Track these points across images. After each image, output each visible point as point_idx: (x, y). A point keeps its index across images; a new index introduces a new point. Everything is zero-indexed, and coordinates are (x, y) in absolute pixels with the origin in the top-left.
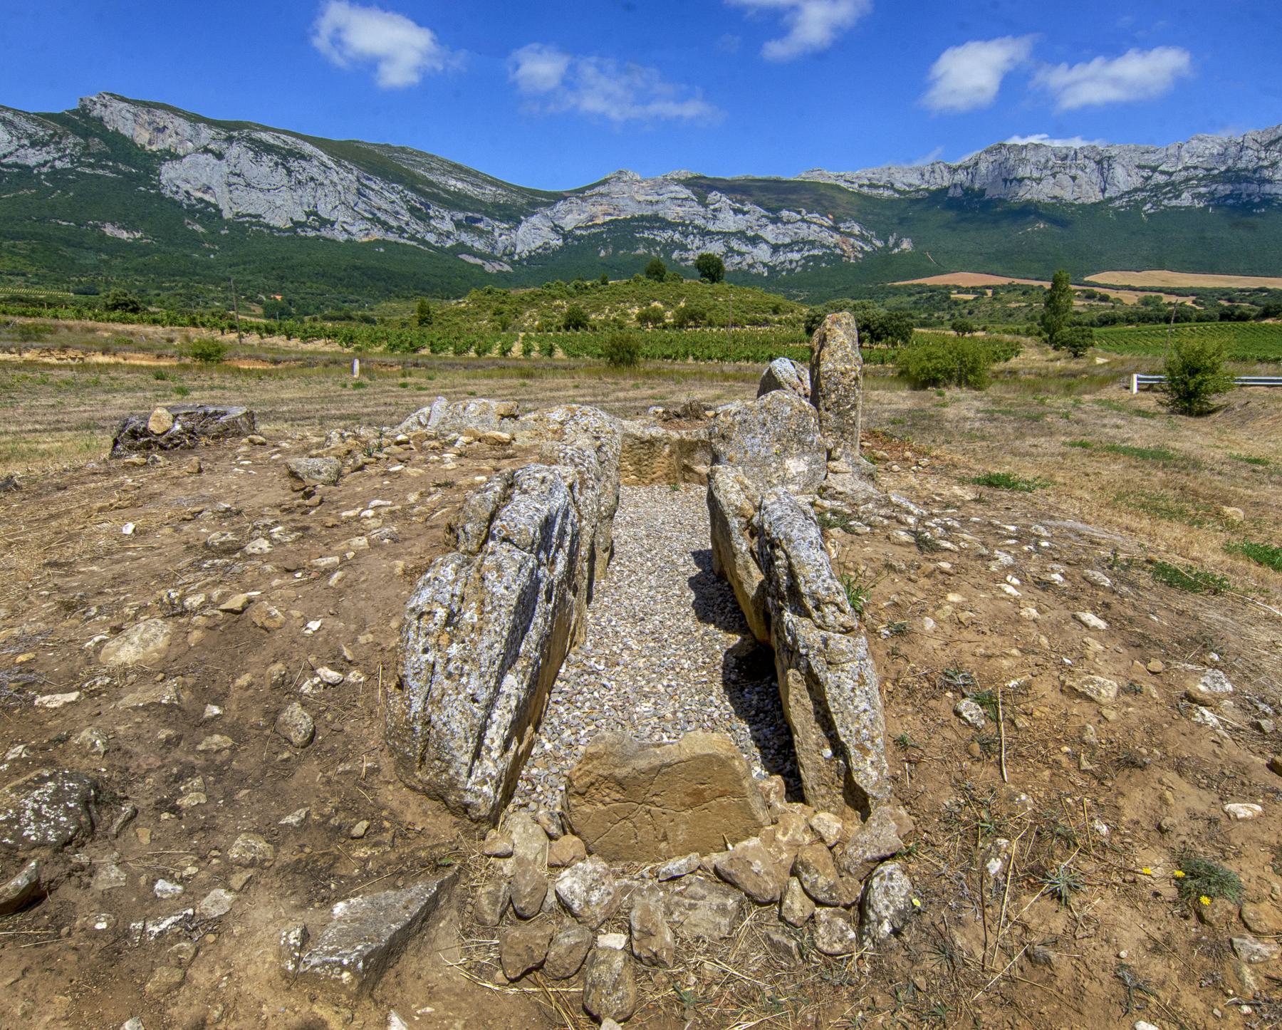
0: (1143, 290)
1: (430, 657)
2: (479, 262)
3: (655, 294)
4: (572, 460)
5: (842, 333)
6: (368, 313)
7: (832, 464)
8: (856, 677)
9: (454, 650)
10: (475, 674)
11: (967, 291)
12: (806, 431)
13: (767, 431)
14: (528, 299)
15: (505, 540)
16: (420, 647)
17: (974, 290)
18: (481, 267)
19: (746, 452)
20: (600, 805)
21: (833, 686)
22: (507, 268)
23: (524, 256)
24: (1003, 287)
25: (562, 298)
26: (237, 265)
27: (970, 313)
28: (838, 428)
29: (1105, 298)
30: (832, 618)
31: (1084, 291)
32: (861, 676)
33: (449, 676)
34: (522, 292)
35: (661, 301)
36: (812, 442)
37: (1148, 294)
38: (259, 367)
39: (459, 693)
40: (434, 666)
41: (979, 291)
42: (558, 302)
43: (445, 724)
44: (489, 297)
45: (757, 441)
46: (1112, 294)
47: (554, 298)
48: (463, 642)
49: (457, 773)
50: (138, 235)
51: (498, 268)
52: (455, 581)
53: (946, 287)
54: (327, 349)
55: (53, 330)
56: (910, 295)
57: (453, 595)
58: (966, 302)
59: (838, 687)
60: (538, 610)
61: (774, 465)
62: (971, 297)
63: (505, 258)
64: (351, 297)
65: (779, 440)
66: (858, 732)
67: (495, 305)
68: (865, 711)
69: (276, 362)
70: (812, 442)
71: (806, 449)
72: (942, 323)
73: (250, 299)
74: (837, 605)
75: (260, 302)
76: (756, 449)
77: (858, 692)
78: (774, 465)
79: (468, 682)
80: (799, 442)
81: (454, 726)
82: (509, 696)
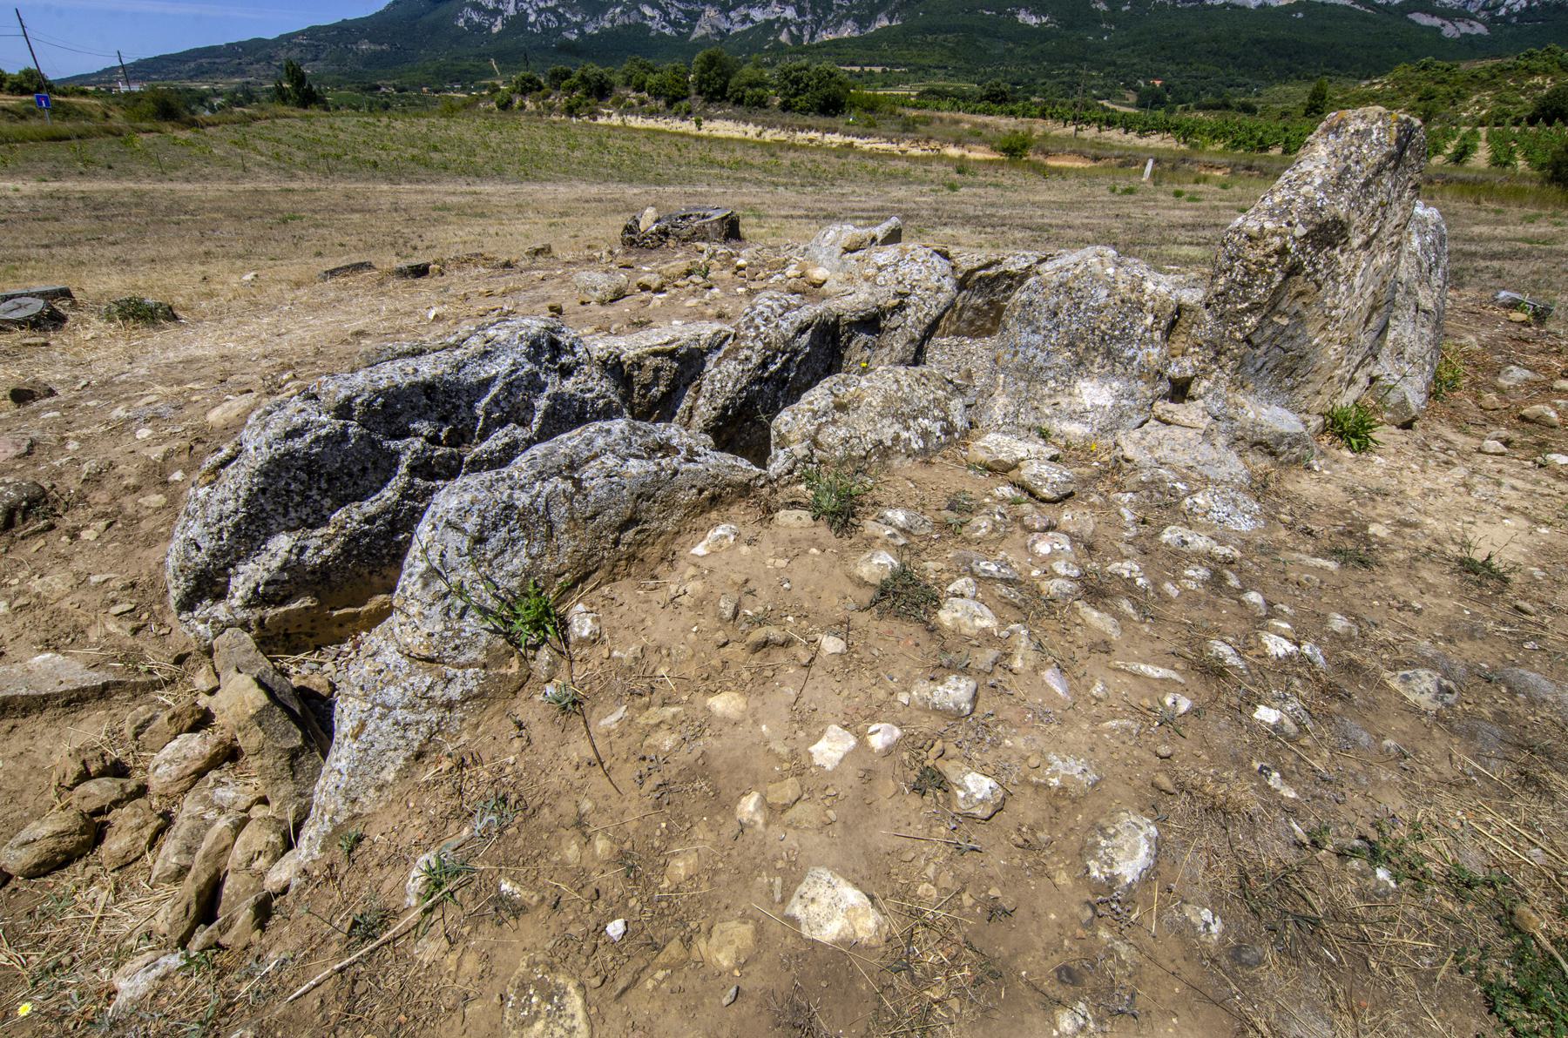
2: (1437, 22)
6: (1252, 100)
12: (1126, 337)
14: (1485, 75)
18: (1438, 30)
19: (1015, 354)
22: (1480, 29)
23: (1517, 8)
26: (1128, 46)
28: (1211, 343)
34: (1477, 65)
36: (1133, 358)
38: (1079, 164)
42: (1538, 80)
44: (1421, 74)
47: (1533, 73)
50: (1044, 20)
51: (1464, 28)
54: (1161, 145)
55: (927, 122)
60: (393, 482)
61: (1052, 384)
63: (1483, 14)
64: (1240, 80)
65: (1072, 344)
67: (1426, 85)
69: (1096, 159)
70: (1133, 358)
71: (1119, 369)
73: (1128, 86)
75: (1136, 90)
76: (1030, 352)
78: (1052, 384)
80: (1108, 354)
82: (274, 555)
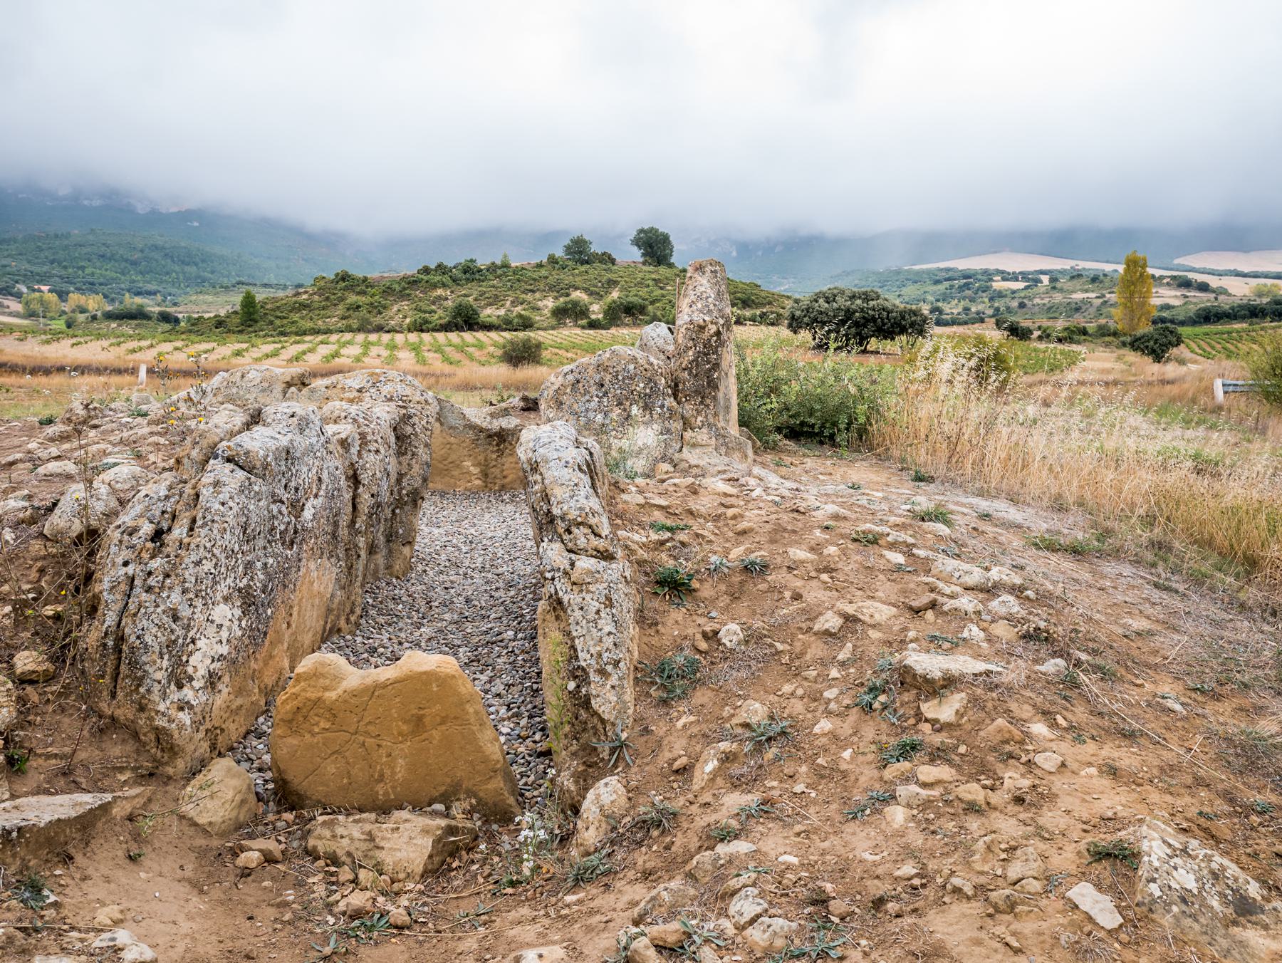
0: (1256, 275)
1: (130, 570)
3: (578, 281)
4: (355, 420)
5: (705, 282)
7: (688, 435)
8: (603, 599)
9: (156, 564)
10: (178, 589)
11: (1014, 277)
13: (606, 394)
15: (229, 460)
16: (120, 560)
17: (1024, 276)
20: (308, 736)
21: (576, 608)
24: (1063, 272)
25: (444, 285)
27: (1022, 305)
28: (697, 392)
29: (1204, 287)
30: (583, 540)
31: (1174, 278)
32: (608, 598)
33: (149, 590)
35: (586, 290)
37: (1262, 281)
39: (157, 606)
40: (133, 579)
41: (1032, 279)
42: (440, 292)
43: (138, 637)
45: (593, 405)
46: (1214, 282)
47: (435, 286)
48: (168, 556)
49: (148, 691)
52: (167, 497)
53: (985, 272)
56: (937, 282)
57: (163, 512)
58: (1014, 292)
59: (582, 609)
62: (1020, 285)
66: (600, 655)
68: (610, 633)
72: (982, 321)
74: (590, 527)
77: (603, 614)
79: (168, 597)
81: (148, 639)
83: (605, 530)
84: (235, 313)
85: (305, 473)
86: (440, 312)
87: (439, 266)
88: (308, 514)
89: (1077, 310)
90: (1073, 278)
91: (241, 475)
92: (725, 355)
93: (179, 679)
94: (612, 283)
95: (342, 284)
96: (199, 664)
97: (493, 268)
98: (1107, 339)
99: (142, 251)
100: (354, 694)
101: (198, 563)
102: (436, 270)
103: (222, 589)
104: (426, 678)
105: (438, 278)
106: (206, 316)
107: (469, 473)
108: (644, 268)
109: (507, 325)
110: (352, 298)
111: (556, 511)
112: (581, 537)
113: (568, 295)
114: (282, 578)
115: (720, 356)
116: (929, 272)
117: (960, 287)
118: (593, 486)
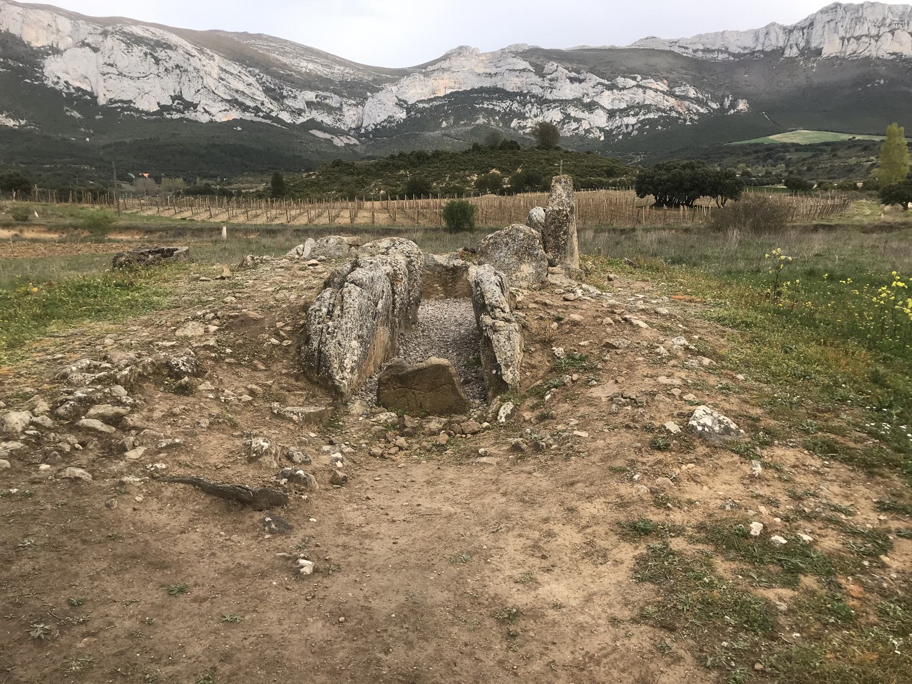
15: (352, 282)
27: (809, 169)
33: (329, 333)
35: (499, 168)
47: (399, 168)
62: (810, 154)
83: (507, 310)
84: (269, 188)
85: (379, 287)
86: (402, 185)
87: (401, 154)
88: (380, 306)
89: (851, 171)
90: (849, 147)
91: (358, 289)
92: (571, 227)
93: (342, 368)
94: (518, 163)
95: (337, 168)
96: (348, 363)
97: (437, 154)
98: (870, 192)
99: (206, 148)
100: (410, 373)
101: (346, 323)
102: (398, 157)
103: (354, 335)
104: (438, 367)
105: (400, 162)
106: (251, 191)
107: (437, 290)
108: (540, 151)
109: (446, 192)
110: (346, 178)
111: (487, 302)
112: (498, 312)
113: (488, 172)
114: (373, 332)
115: (568, 228)
116: (741, 147)
117: (765, 157)
118: (502, 292)
